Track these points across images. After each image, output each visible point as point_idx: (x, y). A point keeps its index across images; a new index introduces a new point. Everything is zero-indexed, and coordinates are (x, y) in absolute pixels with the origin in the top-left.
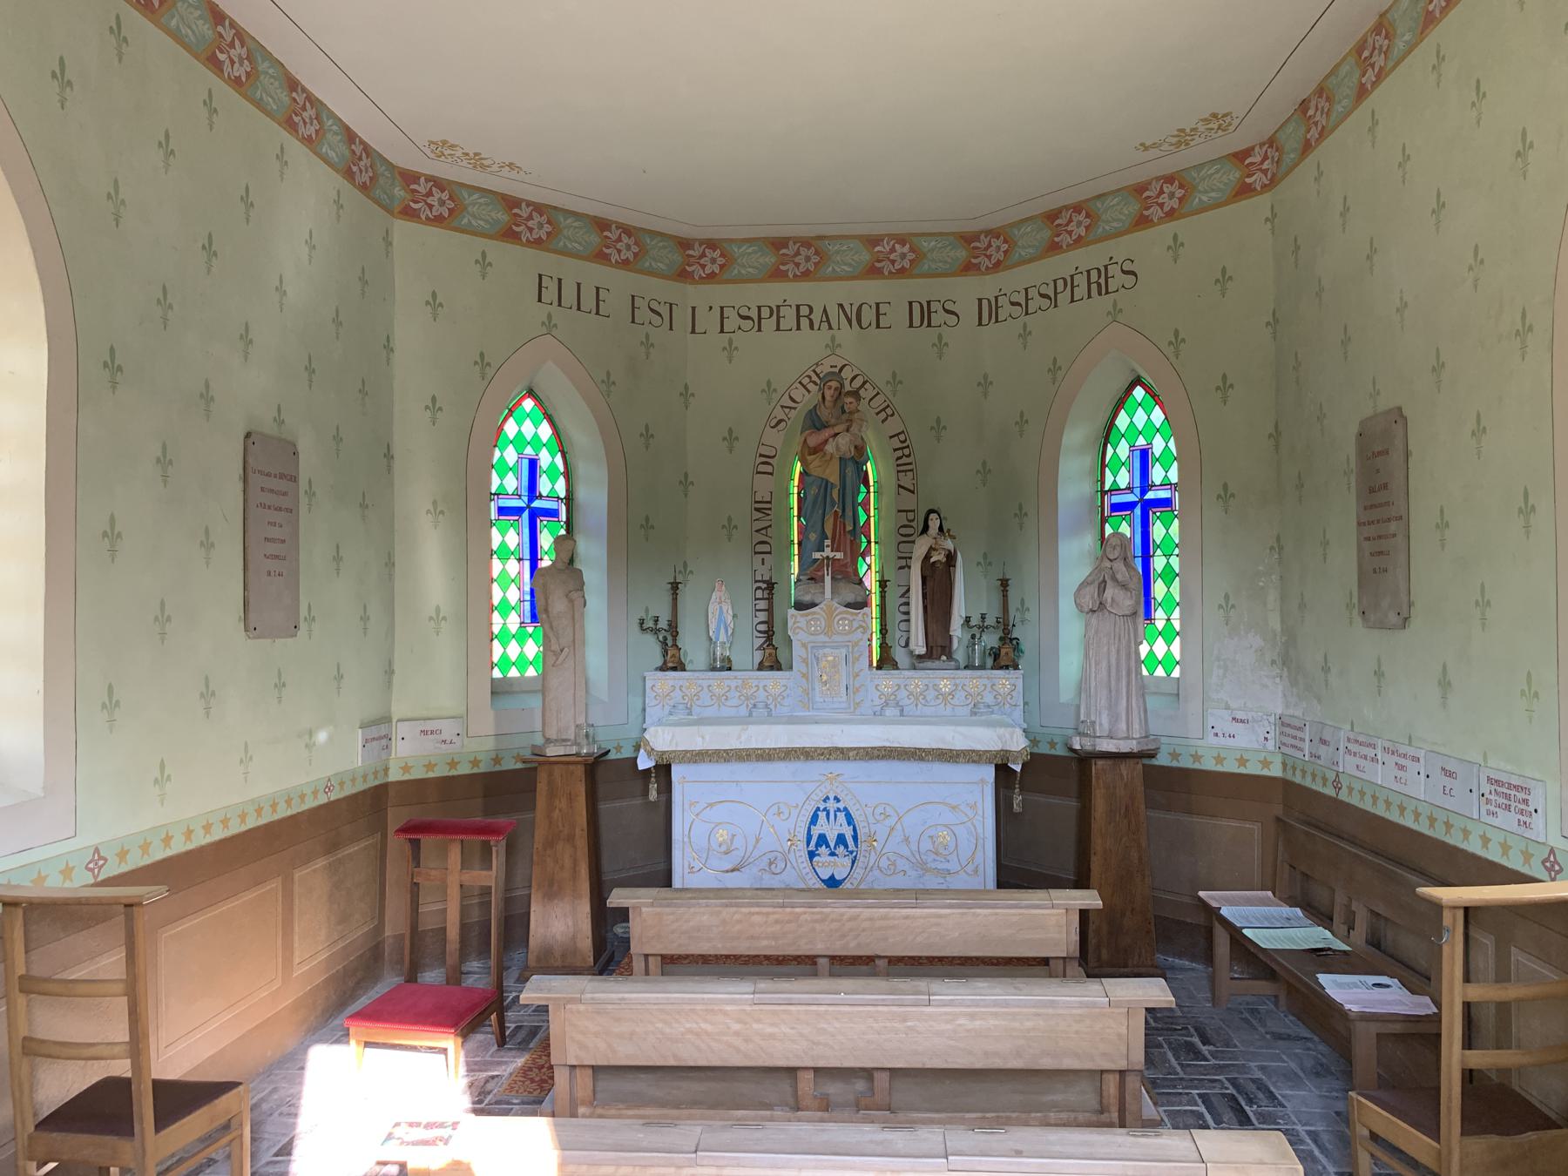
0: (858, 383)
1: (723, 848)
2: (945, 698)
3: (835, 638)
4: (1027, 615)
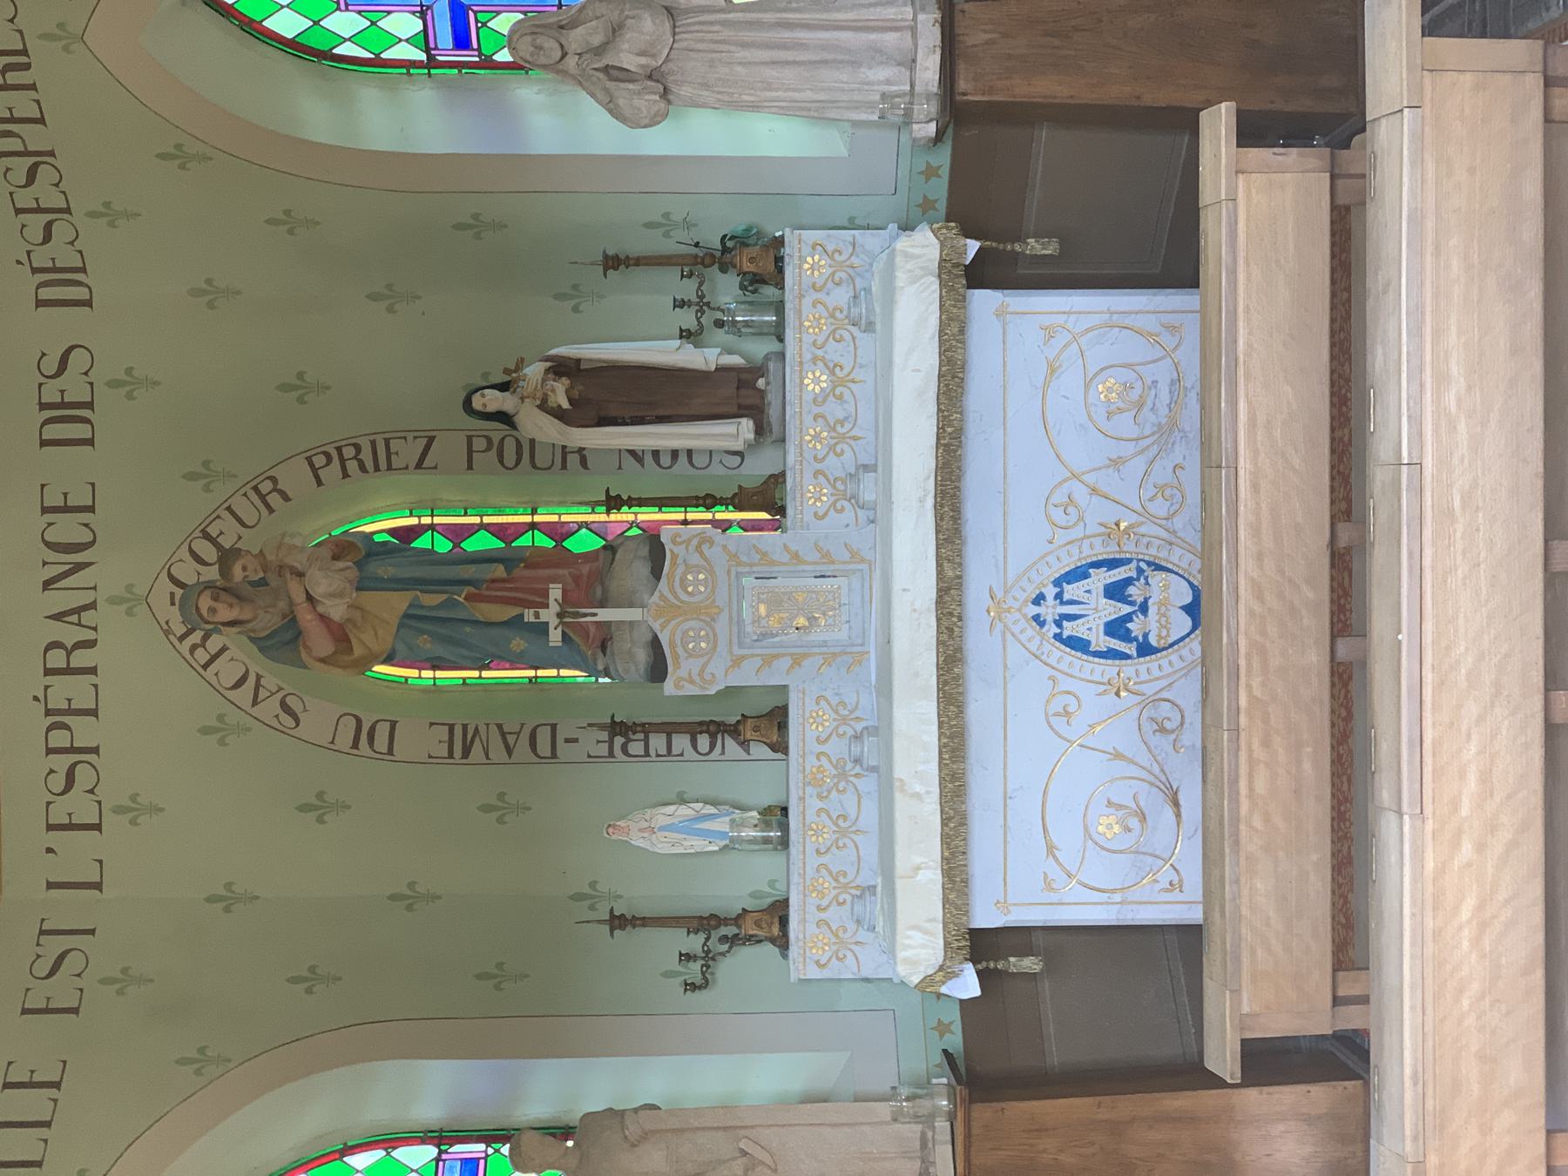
0: (208, 552)
1: (1134, 823)
2: (840, 382)
3: (718, 611)
4: (677, 217)
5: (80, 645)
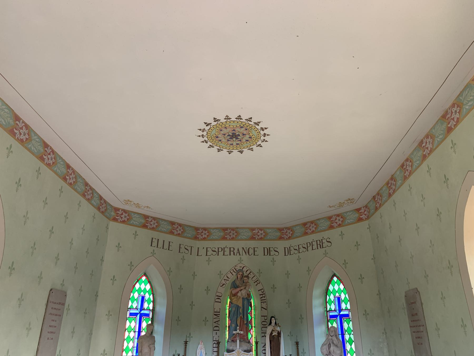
0: (248, 272)
5: (234, 253)
